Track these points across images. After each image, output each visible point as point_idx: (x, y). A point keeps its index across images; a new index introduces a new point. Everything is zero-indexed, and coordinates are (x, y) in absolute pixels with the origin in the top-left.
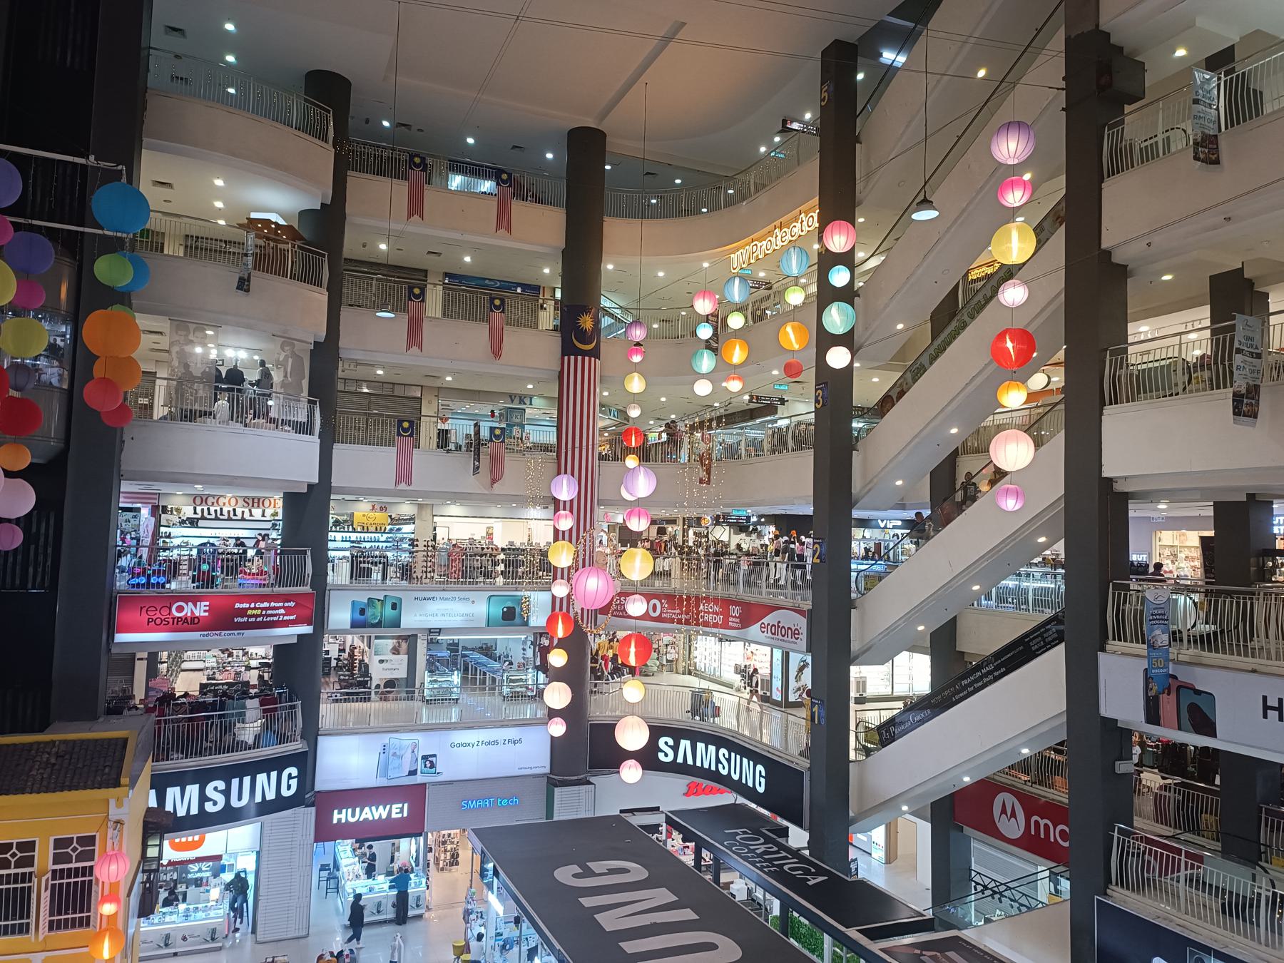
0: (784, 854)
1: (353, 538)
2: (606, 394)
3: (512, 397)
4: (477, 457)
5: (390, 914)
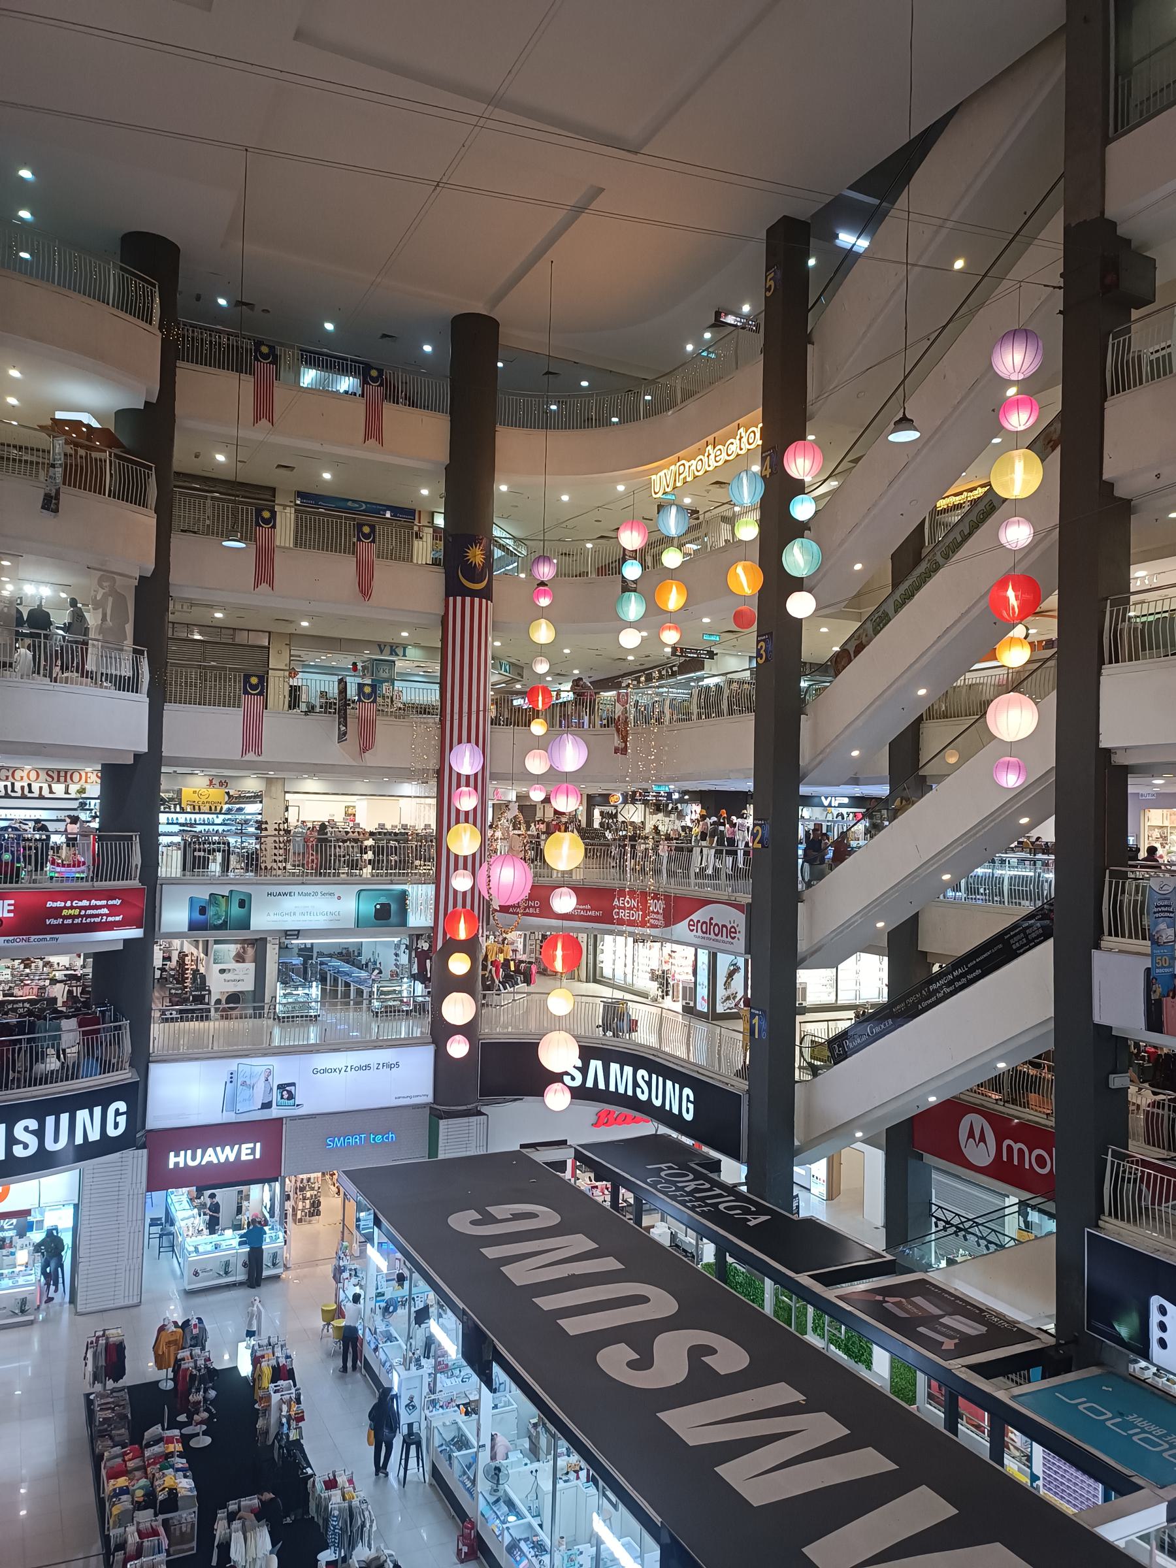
0: (718, 1191)
1: (182, 821)
2: (497, 644)
3: (381, 646)
4: (343, 720)
5: (241, 1275)
